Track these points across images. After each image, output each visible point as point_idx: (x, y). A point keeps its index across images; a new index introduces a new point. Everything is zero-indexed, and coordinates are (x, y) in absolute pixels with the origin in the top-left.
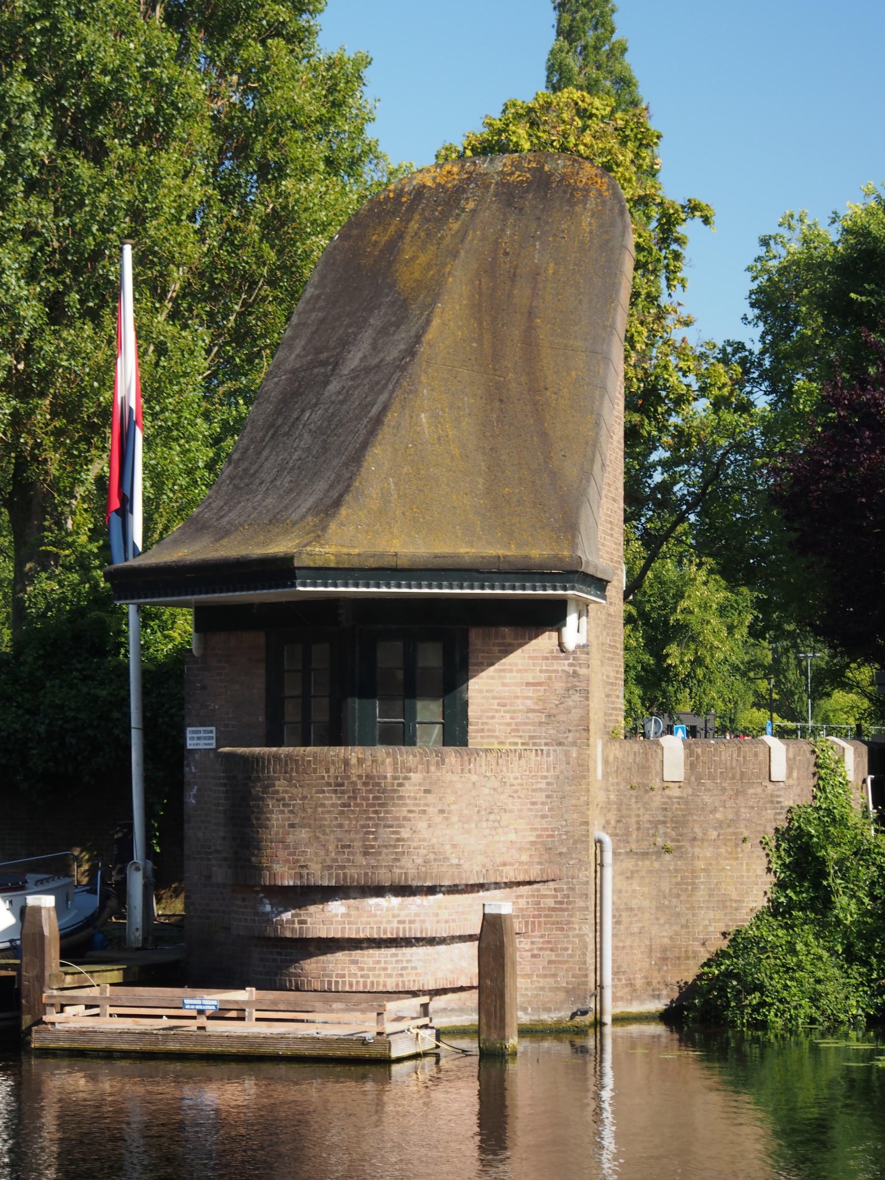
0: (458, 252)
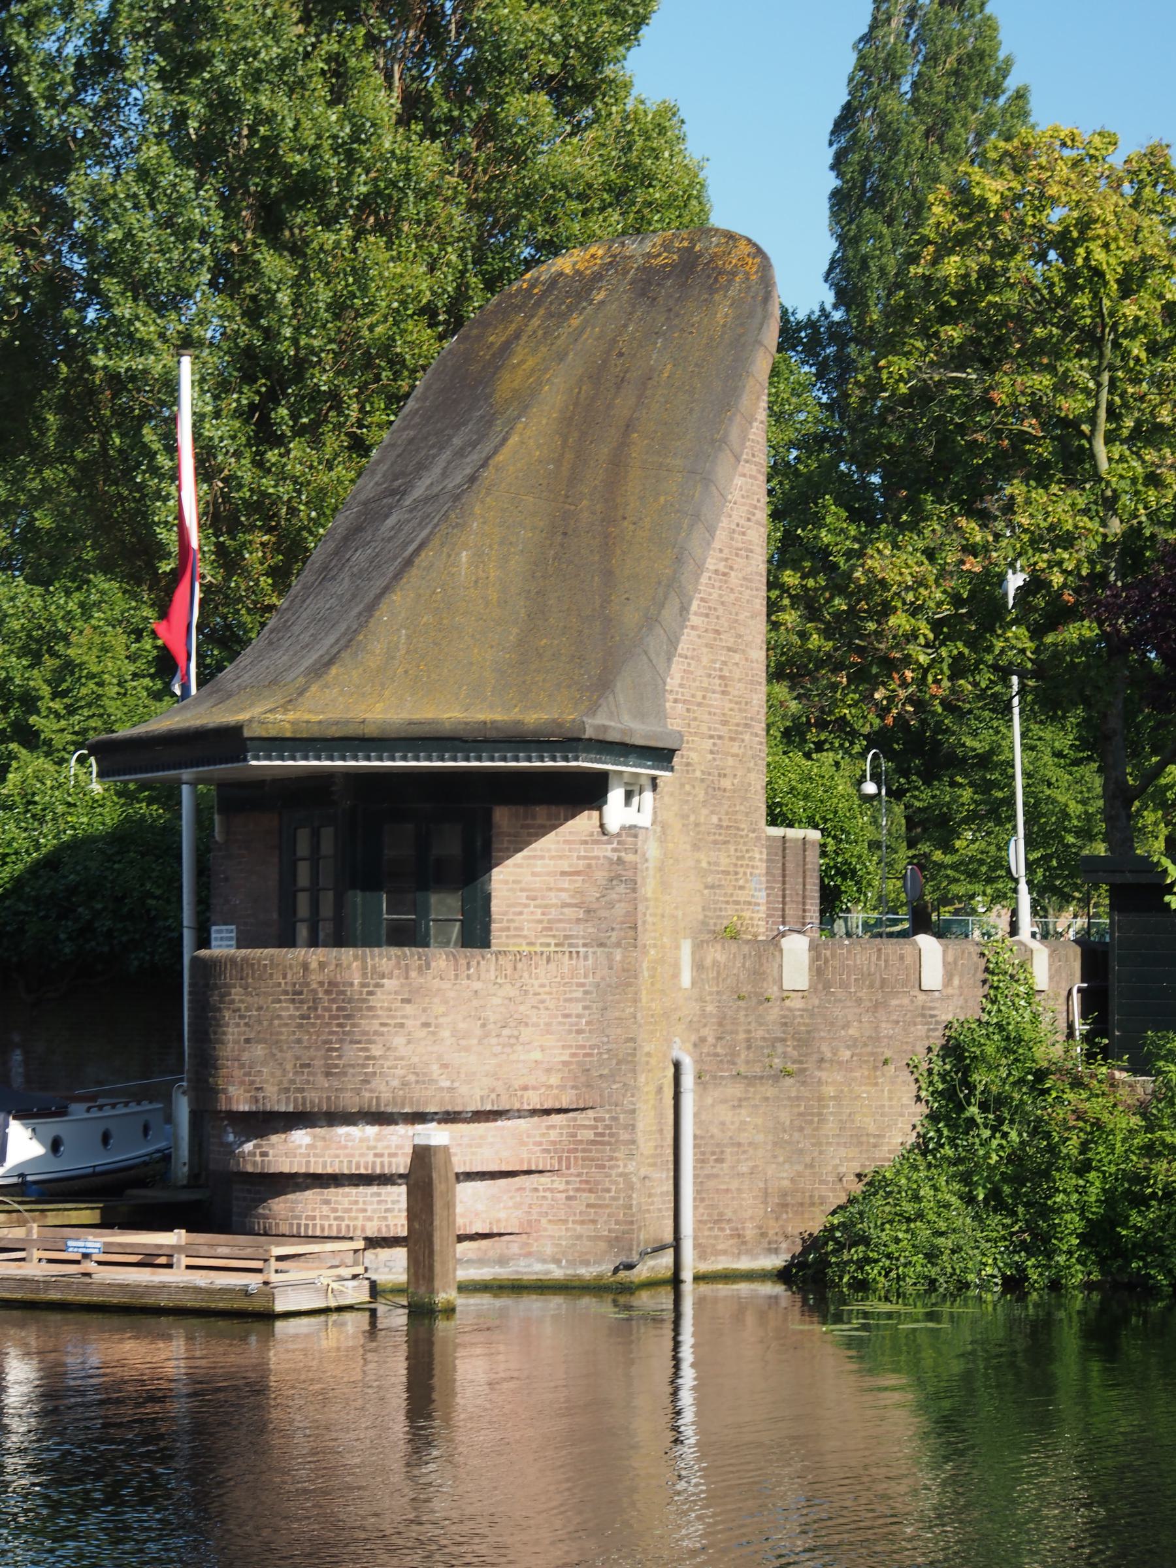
0: (566, 354)
